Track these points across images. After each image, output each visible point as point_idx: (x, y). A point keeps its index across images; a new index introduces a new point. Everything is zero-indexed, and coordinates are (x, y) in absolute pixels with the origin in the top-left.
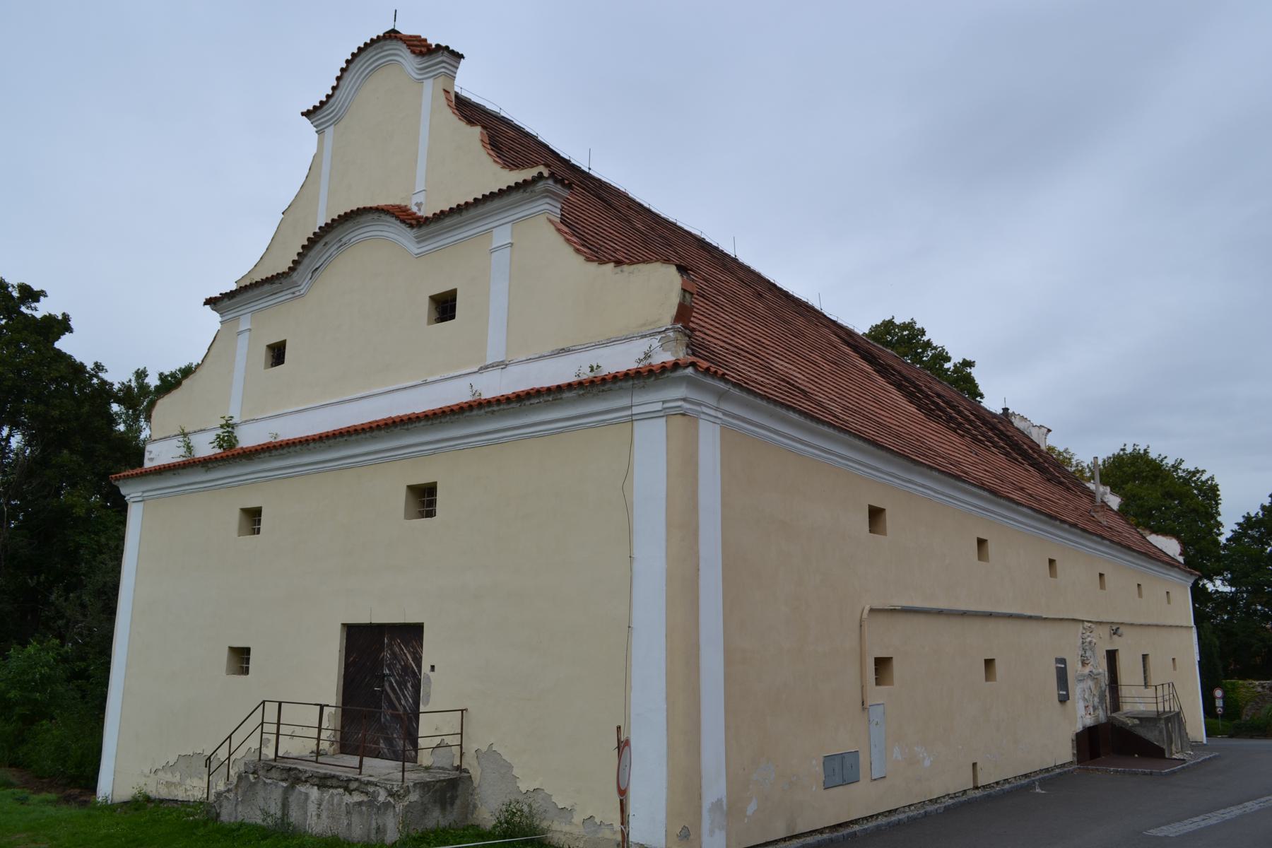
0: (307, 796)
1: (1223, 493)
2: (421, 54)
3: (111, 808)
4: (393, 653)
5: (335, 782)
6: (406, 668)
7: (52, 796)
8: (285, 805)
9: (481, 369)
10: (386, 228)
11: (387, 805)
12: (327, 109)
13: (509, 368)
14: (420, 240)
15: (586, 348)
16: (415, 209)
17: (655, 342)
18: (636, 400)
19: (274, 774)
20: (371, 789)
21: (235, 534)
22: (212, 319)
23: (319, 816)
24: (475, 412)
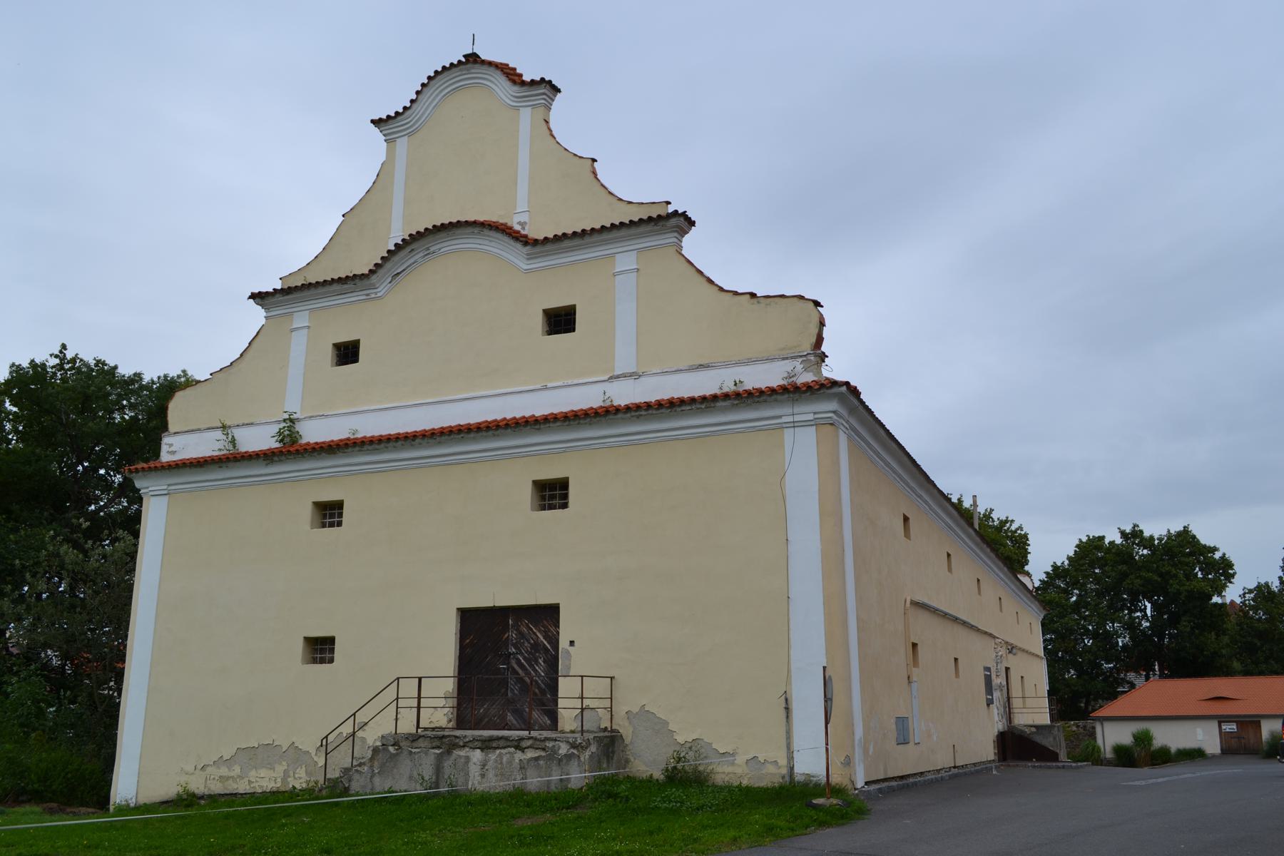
0: (468, 759)
1: (1032, 540)
2: (514, 82)
3: (124, 809)
4: (521, 635)
5: (502, 743)
6: (536, 646)
7: (37, 809)
8: (438, 769)
9: (611, 378)
10: (486, 242)
11: (569, 757)
12: (401, 121)
13: (642, 379)
14: (530, 257)
15: (727, 364)
16: (517, 227)
17: (799, 367)
18: (796, 410)
19: (421, 743)
20: (550, 744)
21: (308, 527)
22: (257, 316)
23: (483, 776)
24: (620, 416)
